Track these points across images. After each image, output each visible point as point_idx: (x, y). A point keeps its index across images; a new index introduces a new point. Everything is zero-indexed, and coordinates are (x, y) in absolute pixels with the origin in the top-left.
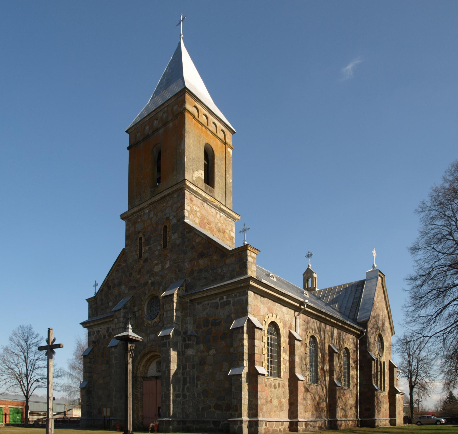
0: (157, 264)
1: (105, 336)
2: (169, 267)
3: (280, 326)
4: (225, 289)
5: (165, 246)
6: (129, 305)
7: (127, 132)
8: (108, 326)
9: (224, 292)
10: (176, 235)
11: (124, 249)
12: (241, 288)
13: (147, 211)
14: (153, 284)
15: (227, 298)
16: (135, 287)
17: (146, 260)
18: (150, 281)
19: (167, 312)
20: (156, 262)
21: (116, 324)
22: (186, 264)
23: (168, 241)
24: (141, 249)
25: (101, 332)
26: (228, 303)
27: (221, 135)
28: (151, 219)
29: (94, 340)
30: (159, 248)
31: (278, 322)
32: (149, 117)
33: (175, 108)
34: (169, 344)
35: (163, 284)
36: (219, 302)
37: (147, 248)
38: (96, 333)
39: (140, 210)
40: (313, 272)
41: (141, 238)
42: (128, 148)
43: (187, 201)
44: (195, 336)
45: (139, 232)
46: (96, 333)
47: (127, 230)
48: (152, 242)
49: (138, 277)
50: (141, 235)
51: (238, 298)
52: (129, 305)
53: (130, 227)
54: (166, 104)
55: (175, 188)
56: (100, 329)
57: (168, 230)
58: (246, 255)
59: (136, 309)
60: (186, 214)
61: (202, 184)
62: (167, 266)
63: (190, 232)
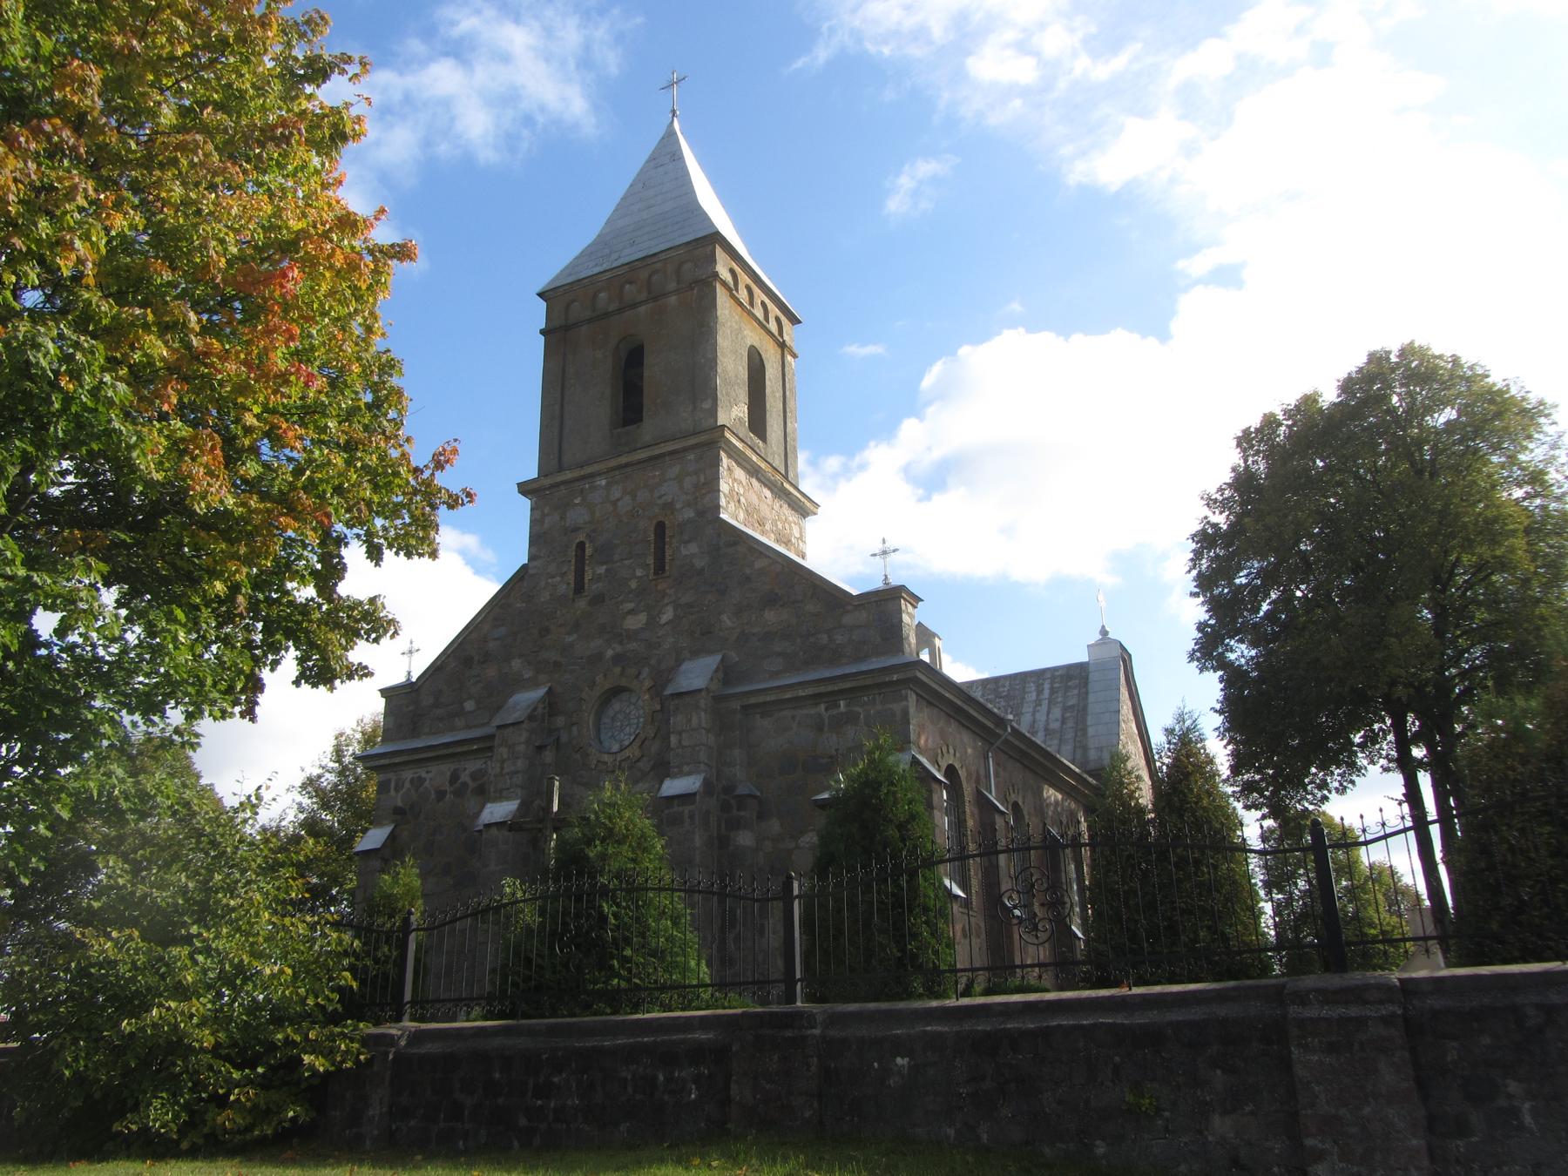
0: (631, 612)
1: (441, 795)
2: (670, 622)
3: (962, 773)
4: (848, 685)
5: (660, 568)
6: (540, 710)
7: (540, 295)
8: (453, 767)
9: (842, 692)
10: (693, 548)
11: (524, 567)
12: (892, 683)
13: (604, 482)
14: (617, 659)
15: (847, 705)
16: (557, 664)
17: (598, 600)
18: (610, 653)
19: (680, 733)
20: (630, 606)
21: (503, 761)
22: (724, 617)
23: (668, 558)
24: (583, 571)
25: (427, 784)
26: (851, 718)
27: (759, 313)
28: (615, 503)
29: (400, 804)
30: (639, 573)
31: (957, 766)
32: (609, 275)
33: (687, 266)
34: (692, 817)
35: (653, 662)
36: (825, 715)
37: (602, 570)
38: (407, 785)
39: (583, 478)
40: (934, 635)
41: (581, 546)
42: (542, 332)
43: (723, 471)
44: (755, 797)
45: (576, 530)
46: (407, 785)
47: (534, 522)
48: (616, 557)
49: (570, 639)
50: (581, 537)
51: (879, 707)
52: (540, 710)
53: (544, 515)
54: (662, 256)
55: (693, 441)
56: (424, 775)
57: (668, 533)
58: (900, 611)
59: (560, 721)
60: (723, 502)
61: (744, 431)
62: (667, 615)
63: (735, 543)
